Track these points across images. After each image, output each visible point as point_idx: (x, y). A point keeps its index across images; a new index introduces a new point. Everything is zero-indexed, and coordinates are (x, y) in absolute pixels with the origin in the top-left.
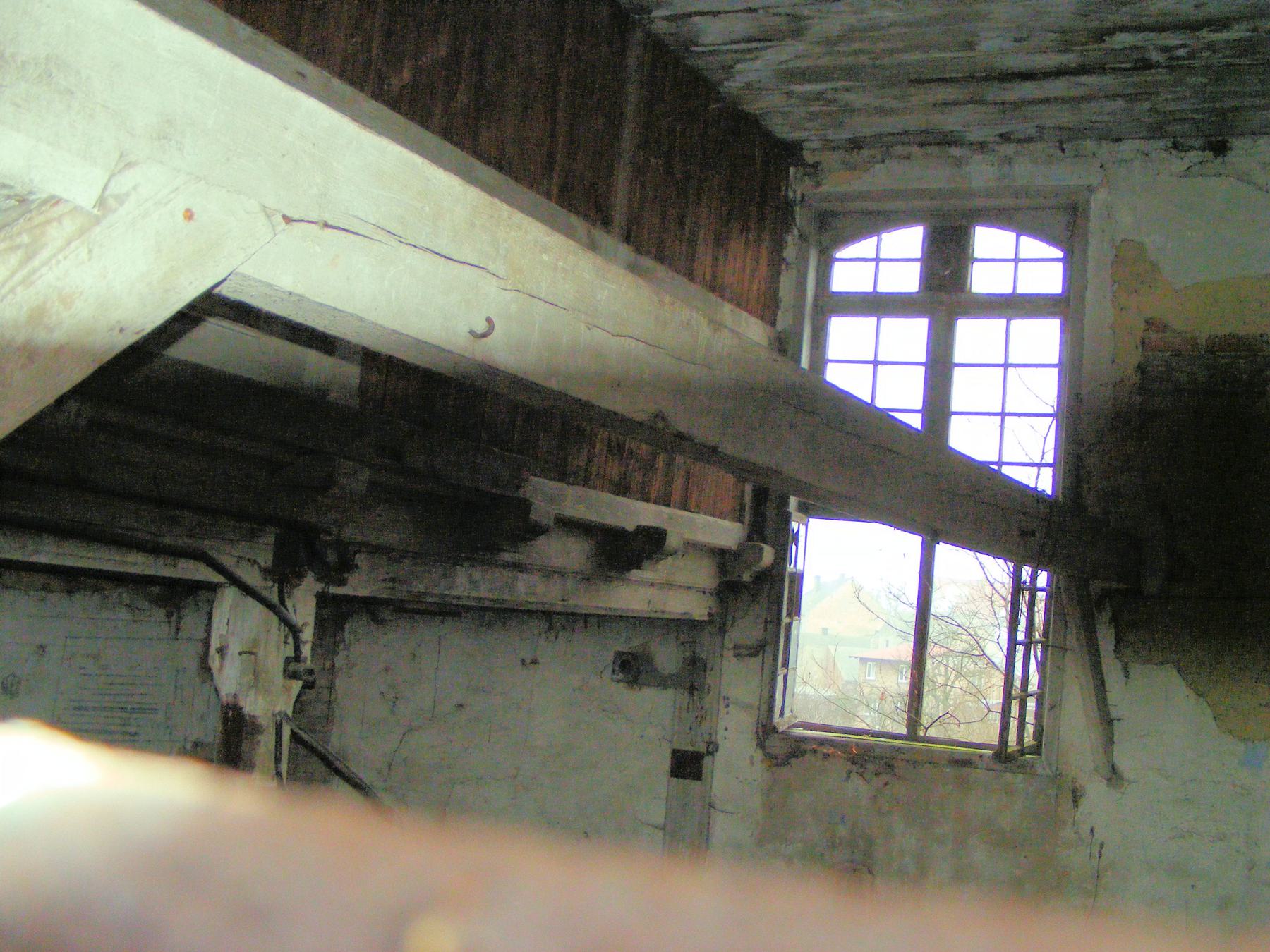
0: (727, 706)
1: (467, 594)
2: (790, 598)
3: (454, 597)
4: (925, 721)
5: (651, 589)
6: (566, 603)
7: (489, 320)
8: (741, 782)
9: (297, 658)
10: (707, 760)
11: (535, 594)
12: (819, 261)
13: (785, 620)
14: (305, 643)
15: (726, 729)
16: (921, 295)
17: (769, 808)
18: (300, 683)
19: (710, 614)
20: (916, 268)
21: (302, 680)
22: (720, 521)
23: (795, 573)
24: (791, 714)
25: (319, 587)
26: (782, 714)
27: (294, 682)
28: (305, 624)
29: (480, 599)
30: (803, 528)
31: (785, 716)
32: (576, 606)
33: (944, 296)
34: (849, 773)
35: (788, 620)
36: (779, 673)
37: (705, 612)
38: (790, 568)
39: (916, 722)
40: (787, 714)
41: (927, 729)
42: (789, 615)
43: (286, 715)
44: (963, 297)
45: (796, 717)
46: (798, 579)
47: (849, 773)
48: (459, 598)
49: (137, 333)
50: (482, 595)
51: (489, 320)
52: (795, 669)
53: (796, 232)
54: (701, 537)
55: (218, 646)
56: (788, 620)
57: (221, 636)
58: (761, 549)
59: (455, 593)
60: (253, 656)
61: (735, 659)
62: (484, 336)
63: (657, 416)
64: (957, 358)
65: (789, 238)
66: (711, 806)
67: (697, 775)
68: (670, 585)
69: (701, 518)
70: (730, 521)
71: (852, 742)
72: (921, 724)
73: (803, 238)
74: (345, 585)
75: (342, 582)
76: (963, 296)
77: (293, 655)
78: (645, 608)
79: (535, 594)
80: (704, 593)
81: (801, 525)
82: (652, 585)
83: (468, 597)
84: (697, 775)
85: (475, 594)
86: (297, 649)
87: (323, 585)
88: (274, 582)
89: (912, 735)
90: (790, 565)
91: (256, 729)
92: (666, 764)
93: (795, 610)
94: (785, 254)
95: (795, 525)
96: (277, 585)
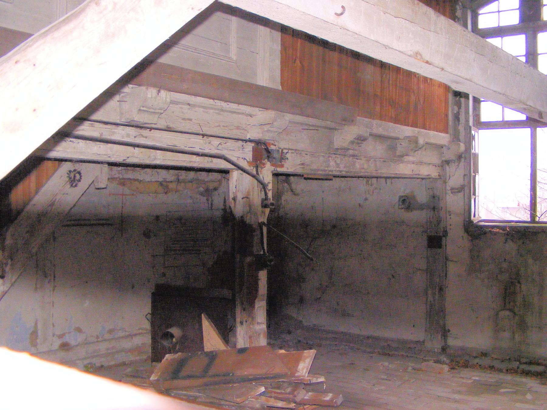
0: (450, 215)
1: (335, 169)
2: (474, 164)
3: (330, 171)
4: (538, 214)
5: (413, 165)
6: (377, 172)
7: (343, 7)
8: (459, 247)
9: (266, 199)
10: (444, 238)
11: (363, 168)
12: (472, 16)
13: (473, 174)
14: (269, 190)
15: (451, 225)
16: (520, 24)
17: (472, 258)
18: (269, 209)
19: (439, 175)
20: (517, 13)
21: (269, 208)
22: (440, 134)
23: (475, 153)
24: (478, 216)
25: (273, 168)
26: (474, 216)
27: (266, 209)
28: (269, 183)
29: (341, 171)
30: (476, 134)
31: (476, 217)
32: (381, 173)
33: (531, 24)
34: (506, 240)
35: (474, 174)
36: (472, 197)
37: (437, 174)
38: (473, 151)
39: (535, 215)
40: (477, 216)
41: (539, 218)
42: (474, 172)
43: (264, 223)
44: (540, 23)
45: (481, 217)
46: (476, 156)
47: (506, 240)
48: (332, 171)
49: (199, 10)
50: (341, 170)
51: (343, 7)
52: (478, 196)
53: (460, 4)
54: (432, 141)
55: (233, 197)
56: (474, 174)
57: (234, 193)
58: (460, 144)
59: (329, 169)
60: (248, 199)
61: (452, 194)
62: (342, 14)
63: (417, 53)
64: (539, 52)
65: (458, 7)
66: (447, 259)
67: (440, 247)
68: (421, 163)
69: (432, 133)
70: (444, 133)
71: (507, 226)
72: (537, 216)
73: (464, 7)
74: (283, 167)
75: (282, 166)
76: (540, 23)
77: (265, 198)
78: (411, 173)
79: (363, 168)
80: (436, 166)
81: (476, 132)
82: (413, 163)
83: (335, 171)
84: (440, 247)
85: (338, 169)
86: (266, 194)
87: (274, 168)
88: (254, 167)
89: (533, 220)
90: (473, 150)
91: (253, 230)
92: (425, 243)
93: (476, 171)
94: (457, 14)
95: (473, 132)
96: (255, 168)
